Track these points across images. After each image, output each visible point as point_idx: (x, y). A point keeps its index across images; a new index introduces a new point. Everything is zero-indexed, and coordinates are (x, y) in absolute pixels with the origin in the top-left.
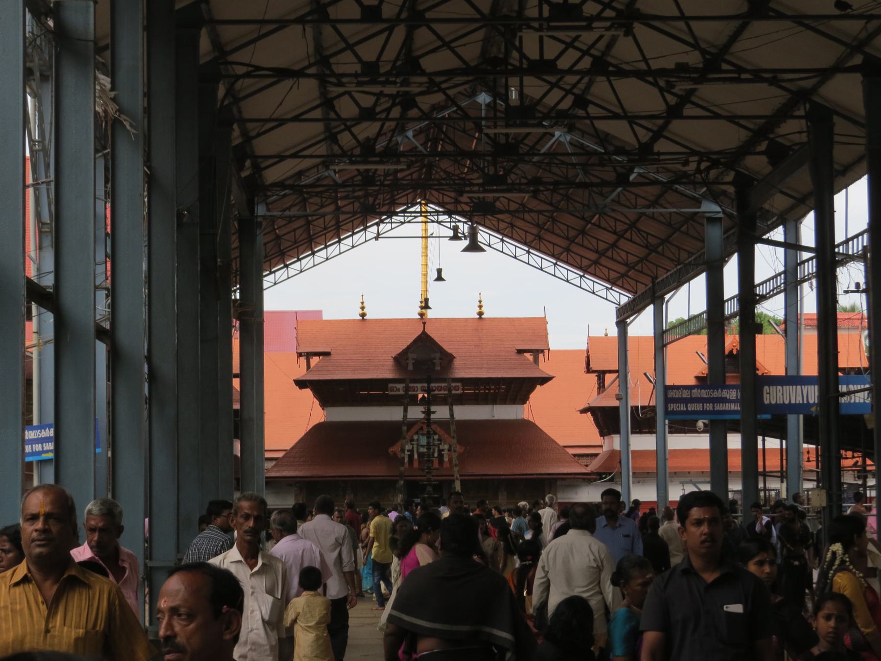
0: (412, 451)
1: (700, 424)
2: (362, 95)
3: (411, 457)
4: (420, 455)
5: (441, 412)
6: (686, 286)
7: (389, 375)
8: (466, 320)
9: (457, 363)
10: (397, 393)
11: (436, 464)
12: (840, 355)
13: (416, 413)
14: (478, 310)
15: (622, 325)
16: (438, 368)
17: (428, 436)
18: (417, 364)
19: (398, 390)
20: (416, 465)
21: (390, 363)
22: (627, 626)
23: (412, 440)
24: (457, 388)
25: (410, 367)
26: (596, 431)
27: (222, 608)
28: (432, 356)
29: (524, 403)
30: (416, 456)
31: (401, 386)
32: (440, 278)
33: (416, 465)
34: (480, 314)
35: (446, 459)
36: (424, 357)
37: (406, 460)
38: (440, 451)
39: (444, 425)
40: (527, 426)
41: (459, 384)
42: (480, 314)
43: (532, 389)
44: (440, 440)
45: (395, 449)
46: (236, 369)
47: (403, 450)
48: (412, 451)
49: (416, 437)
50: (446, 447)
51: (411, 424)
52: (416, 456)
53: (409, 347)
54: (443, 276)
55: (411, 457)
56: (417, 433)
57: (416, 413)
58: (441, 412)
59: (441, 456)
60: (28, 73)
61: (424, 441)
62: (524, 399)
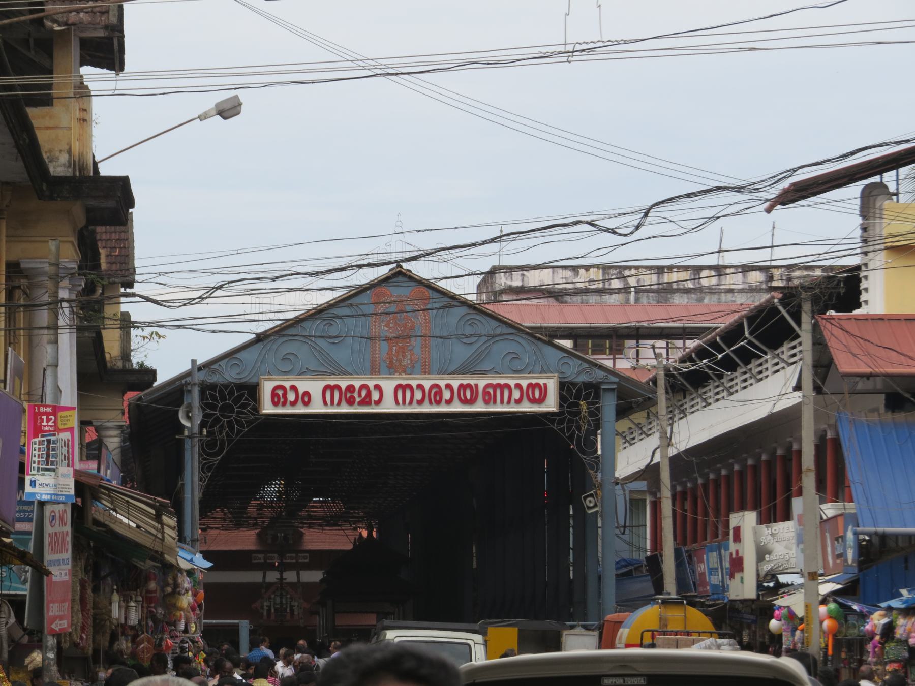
0: (270, 607)
1: (79, 500)
3: (269, 611)
4: (276, 610)
5: (290, 576)
6: (775, 411)
7: (252, 547)
10: (300, 410)
11: (288, 617)
13: (272, 576)
16: (291, 542)
17: (281, 596)
19: (306, 398)
20: (273, 617)
23: (270, 598)
24: (305, 558)
30: (273, 610)
31: (261, 556)
35: (296, 613)
37: (265, 614)
38: (292, 607)
44: (291, 598)
46: (571, 546)
47: (262, 607)
48: (270, 607)
50: (296, 604)
51: (271, 585)
52: (273, 610)
55: (269, 611)
56: (274, 593)
57: (272, 576)
58: (290, 576)
59: (292, 611)
61: (278, 600)
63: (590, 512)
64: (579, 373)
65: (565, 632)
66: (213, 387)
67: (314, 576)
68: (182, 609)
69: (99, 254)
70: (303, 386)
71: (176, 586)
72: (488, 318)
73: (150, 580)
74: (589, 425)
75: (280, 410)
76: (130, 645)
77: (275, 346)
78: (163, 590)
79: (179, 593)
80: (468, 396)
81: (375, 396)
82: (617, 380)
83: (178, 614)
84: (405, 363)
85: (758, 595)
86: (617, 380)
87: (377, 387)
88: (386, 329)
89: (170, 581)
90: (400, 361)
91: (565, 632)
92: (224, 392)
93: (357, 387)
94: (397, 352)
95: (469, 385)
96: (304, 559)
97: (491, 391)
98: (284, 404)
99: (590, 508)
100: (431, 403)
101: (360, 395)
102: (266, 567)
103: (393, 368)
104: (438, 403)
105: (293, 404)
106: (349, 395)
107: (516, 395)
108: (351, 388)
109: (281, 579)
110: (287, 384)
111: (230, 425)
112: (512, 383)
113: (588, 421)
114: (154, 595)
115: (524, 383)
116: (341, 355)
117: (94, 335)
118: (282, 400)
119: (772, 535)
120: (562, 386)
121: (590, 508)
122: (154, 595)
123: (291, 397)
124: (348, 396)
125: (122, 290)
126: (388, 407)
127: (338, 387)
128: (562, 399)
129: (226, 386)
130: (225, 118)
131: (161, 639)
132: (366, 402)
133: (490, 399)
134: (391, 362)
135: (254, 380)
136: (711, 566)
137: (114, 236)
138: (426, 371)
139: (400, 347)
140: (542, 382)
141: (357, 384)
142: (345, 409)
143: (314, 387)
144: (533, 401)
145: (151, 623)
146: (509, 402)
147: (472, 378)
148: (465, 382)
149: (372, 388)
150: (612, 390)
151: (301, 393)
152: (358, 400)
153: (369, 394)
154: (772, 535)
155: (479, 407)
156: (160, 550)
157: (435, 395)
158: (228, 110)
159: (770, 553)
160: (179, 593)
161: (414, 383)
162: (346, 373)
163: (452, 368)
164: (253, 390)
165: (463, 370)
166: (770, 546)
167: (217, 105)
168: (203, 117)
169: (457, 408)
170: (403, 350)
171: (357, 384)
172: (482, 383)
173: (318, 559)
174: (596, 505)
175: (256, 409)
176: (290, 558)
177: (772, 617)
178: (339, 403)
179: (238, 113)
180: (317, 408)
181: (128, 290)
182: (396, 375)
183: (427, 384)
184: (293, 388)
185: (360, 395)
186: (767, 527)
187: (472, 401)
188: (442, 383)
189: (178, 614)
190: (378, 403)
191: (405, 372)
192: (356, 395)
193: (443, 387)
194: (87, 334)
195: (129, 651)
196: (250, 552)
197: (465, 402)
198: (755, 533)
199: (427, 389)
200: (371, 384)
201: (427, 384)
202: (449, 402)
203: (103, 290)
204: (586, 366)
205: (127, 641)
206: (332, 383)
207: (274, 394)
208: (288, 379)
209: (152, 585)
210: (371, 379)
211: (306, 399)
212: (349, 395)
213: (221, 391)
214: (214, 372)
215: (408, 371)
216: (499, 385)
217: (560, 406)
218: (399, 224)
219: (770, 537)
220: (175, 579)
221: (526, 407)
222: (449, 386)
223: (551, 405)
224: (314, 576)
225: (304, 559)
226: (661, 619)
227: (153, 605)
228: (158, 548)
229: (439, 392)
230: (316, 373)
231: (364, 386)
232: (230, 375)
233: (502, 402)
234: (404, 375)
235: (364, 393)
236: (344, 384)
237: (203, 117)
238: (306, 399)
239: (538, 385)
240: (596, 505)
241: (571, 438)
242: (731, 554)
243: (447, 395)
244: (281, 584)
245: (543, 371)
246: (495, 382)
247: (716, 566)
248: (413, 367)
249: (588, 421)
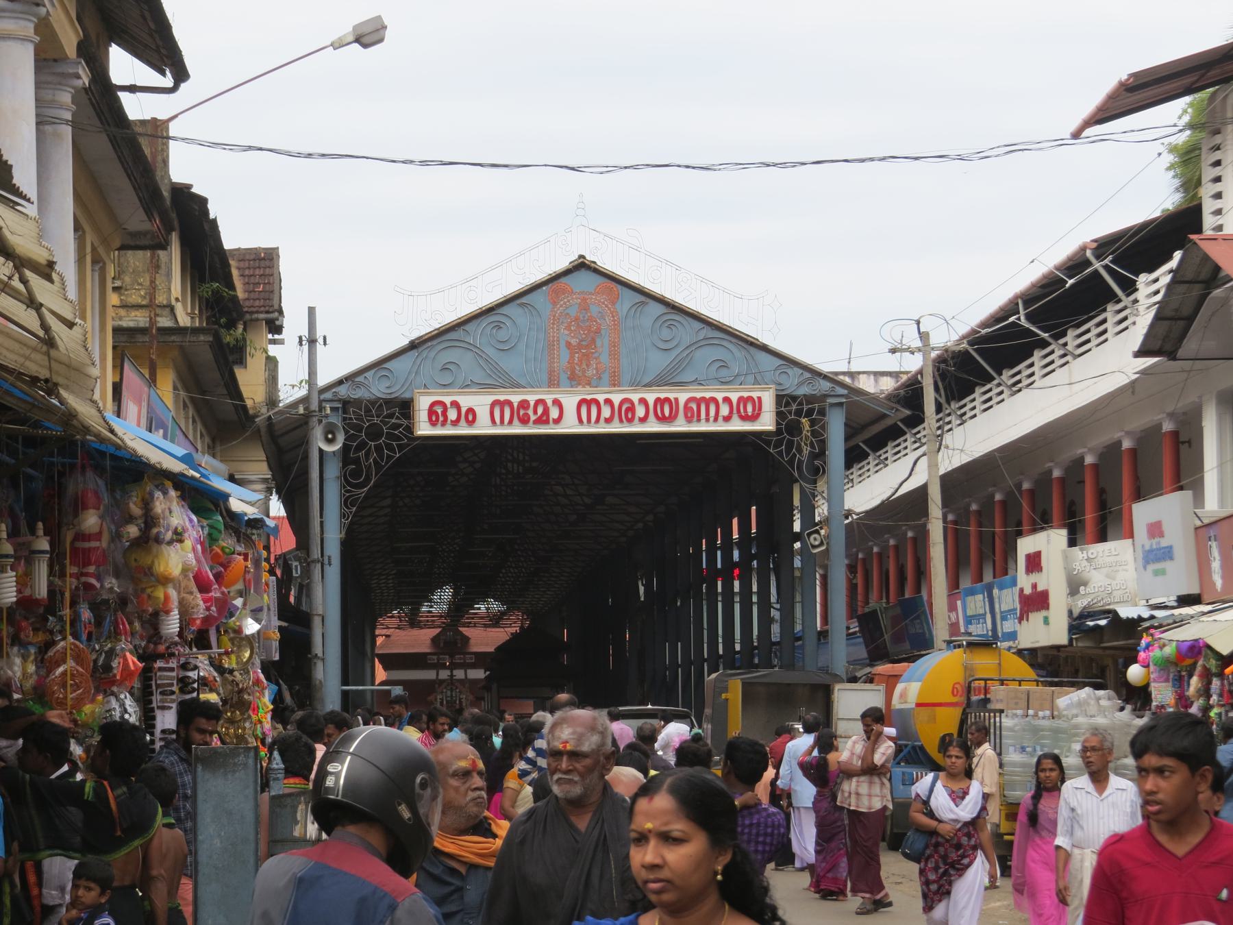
2: (140, 83)
5: (459, 674)
7: (428, 651)
9: (472, 642)
10: (463, 430)
12: (1145, 331)
13: (444, 674)
21: (429, 642)
22: (965, 345)
27: (492, 743)
32: (368, 36)
45: (430, 698)
51: (443, 681)
57: (444, 674)
59: (461, 702)
60: (789, 796)
61: (449, 693)
63: (815, 551)
64: (800, 384)
65: (837, 687)
66: (357, 403)
67: (479, 674)
68: (165, 580)
69: (229, 266)
70: (466, 401)
71: (150, 521)
72: (690, 319)
73: (85, 507)
74: (812, 446)
75: (439, 431)
76: (31, 668)
77: (432, 354)
78: (117, 536)
79: (158, 540)
80: (667, 413)
81: (554, 413)
82: (845, 392)
83: (160, 593)
84: (589, 373)
85: (1071, 640)
86: (845, 392)
87: (557, 402)
88: (567, 332)
89: (136, 510)
90: (584, 372)
91: (837, 687)
92: (371, 418)
93: (532, 403)
94: (580, 361)
95: (667, 400)
96: (470, 660)
97: (694, 406)
98: (444, 423)
99: (814, 547)
100: (621, 421)
101: (535, 412)
102: (439, 666)
103: (575, 379)
104: (630, 421)
105: (456, 423)
106: (522, 412)
107: (724, 410)
108: (524, 404)
109: (452, 676)
110: (448, 400)
111: (379, 449)
112: (719, 396)
113: (812, 443)
114: (94, 544)
115: (734, 397)
116: (511, 364)
117: (211, 339)
118: (441, 419)
119: (1088, 560)
120: (780, 399)
121: (814, 547)
122: (94, 544)
123: (452, 414)
124: (521, 412)
125: (270, 336)
126: (570, 426)
127: (510, 403)
128: (780, 415)
129: (373, 402)
130: (365, 46)
131: (111, 654)
132: (543, 420)
133: (692, 416)
134: (573, 372)
135: (407, 395)
136: (969, 613)
137: (257, 272)
138: (615, 383)
139: (584, 355)
140: (755, 395)
141: (532, 399)
142: (517, 429)
143: (480, 402)
144: (745, 418)
145: (86, 614)
146: (716, 419)
147: (671, 391)
148: (662, 396)
149: (549, 403)
150: (841, 404)
151: (464, 410)
152: (533, 418)
153: (546, 411)
154: (1088, 560)
155: (680, 426)
156: (44, 374)
157: (627, 411)
158: (368, 36)
159: (1085, 584)
160: (158, 540)
161: (601, 398)
162: (519, 386)
163: (647, 380)
164: (406, 407)
165: (661, 381)
166: (1086, 575)
167: (355, 28)
168: (338, 45)
169: (653, 427)
170: (587, 357)
171: (532, 399)
172: (683, 397)
173: (481, 660)
174: (822, 544)
175: (410, 429)
176: (458, 659)
177: (1134, 660)
178: (511, 422)
179: (381, 40)
180: (484, 427)
181: (276, 337)
182: (580, 388)
183: (616, 399)
184: (455, 404)
185: (535, 412)
186: (1082, 550)
187: (671, 418)
188: (635, 397)
189: (160, 593)
190: (557, 421)
191: (589, 384)
192: (530, 412)
193: (636, 402)
194: (202, 338)
195: (29, 684)
196: (425, 655)
197: (662, 419)
198: (1066, 557)
199: (616, 405)
200: (549, 399)
201: (616, 399)
202: (643, 420)
203: (245, 329)
204: (808, 375)
205: (25, 658)
206: (502, 398)
207: (431, 412)
208: (449, 394)
209: (91, 521)
210: (549, 393)
211: (470, 418)
212: (522, 412)
213: (368, 411)
214: (359, 385)
215: (594, 383)
216: (703, 399)
217: (778, 424)
218: (581, 205)
219: (1085, 563)
220: (147, 504)
221: (737, 426)
222: (643, 401)
223: (766, 423)
224: (479, 674)
225: (470, 660)
226: (966, 668)
227: (92, 569)
228: (37, 367)
229: (632, 409)
230: (485, 387)
231: (538, 402)
232: (378, 389)
233: (707, 420)
234: (588, 388)
235: (540, 410)
236: (516, 399)
237: (338, 45)
238: (470, 418)
239: (750, 398)
240: (822, 544)
241: (791, 462)
242: (1022, 590)
243: (640, 411)
244: (452, 681)
245: (756, 382)
246: (698, 395)
247: (982, 611)
248: (600, 378)
249: (812, 443)
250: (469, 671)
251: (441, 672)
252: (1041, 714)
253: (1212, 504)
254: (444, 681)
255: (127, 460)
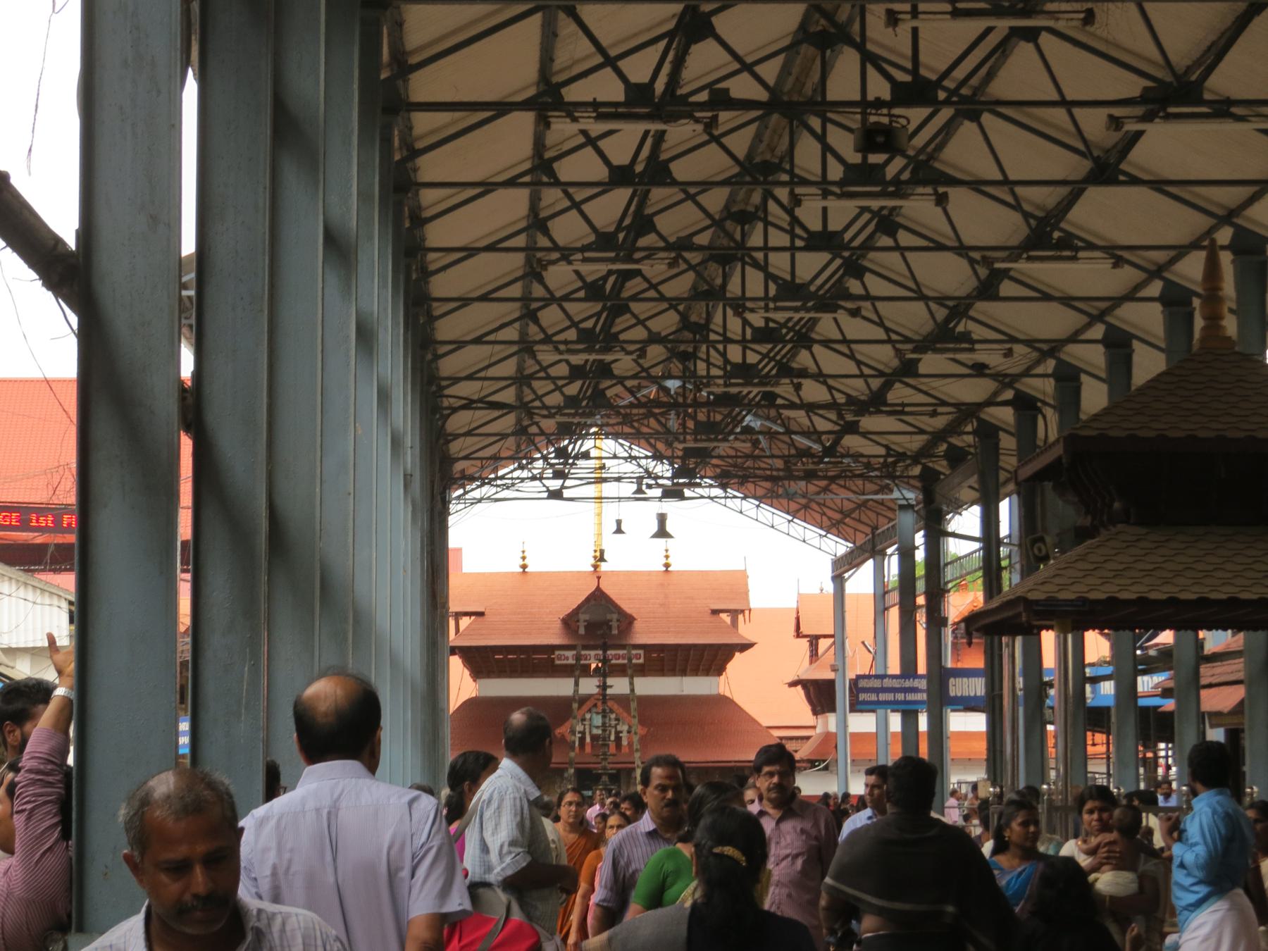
3: (582, 739)
5: (619, 686)
8: (650, 573)
9: (638, 625)
13: (589, 686)
14: (664, 561)
15: (839, 580)
18: (591, 626)
19: (567, 658)
21: (558, 625)
23: (583, 720)
25: (582, 631)
26: (807, 708)
28: (609, 617)
29: (720, 674)
30: (588, 739)
31: (570, 654)
32: (619, 531)
33: (588, 749)
34: (667, 565)
36: (599, 621)
39: (623, 700)
40: (723, 702)
41: (641, 652)
42: (667, 565)
43: (730, 657)
48: (583, 733)
49: (588, 716)
51: (583, 700)
52: (588, 739)
53: (579, 607)
54: (623, 528)
57: (589, 686)
61: (598, 720)
62: (720, 671)
158: (619, 531)
196: (551, 649)
250: (637, 680)
251: (582, 681)
252: (1097, 744)
253: (1254, 791)
254: (589, 697)
255: (1220, 38)
